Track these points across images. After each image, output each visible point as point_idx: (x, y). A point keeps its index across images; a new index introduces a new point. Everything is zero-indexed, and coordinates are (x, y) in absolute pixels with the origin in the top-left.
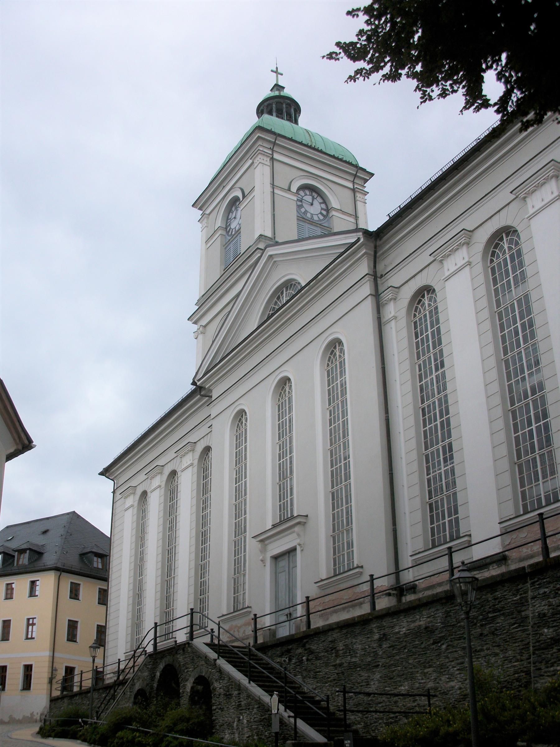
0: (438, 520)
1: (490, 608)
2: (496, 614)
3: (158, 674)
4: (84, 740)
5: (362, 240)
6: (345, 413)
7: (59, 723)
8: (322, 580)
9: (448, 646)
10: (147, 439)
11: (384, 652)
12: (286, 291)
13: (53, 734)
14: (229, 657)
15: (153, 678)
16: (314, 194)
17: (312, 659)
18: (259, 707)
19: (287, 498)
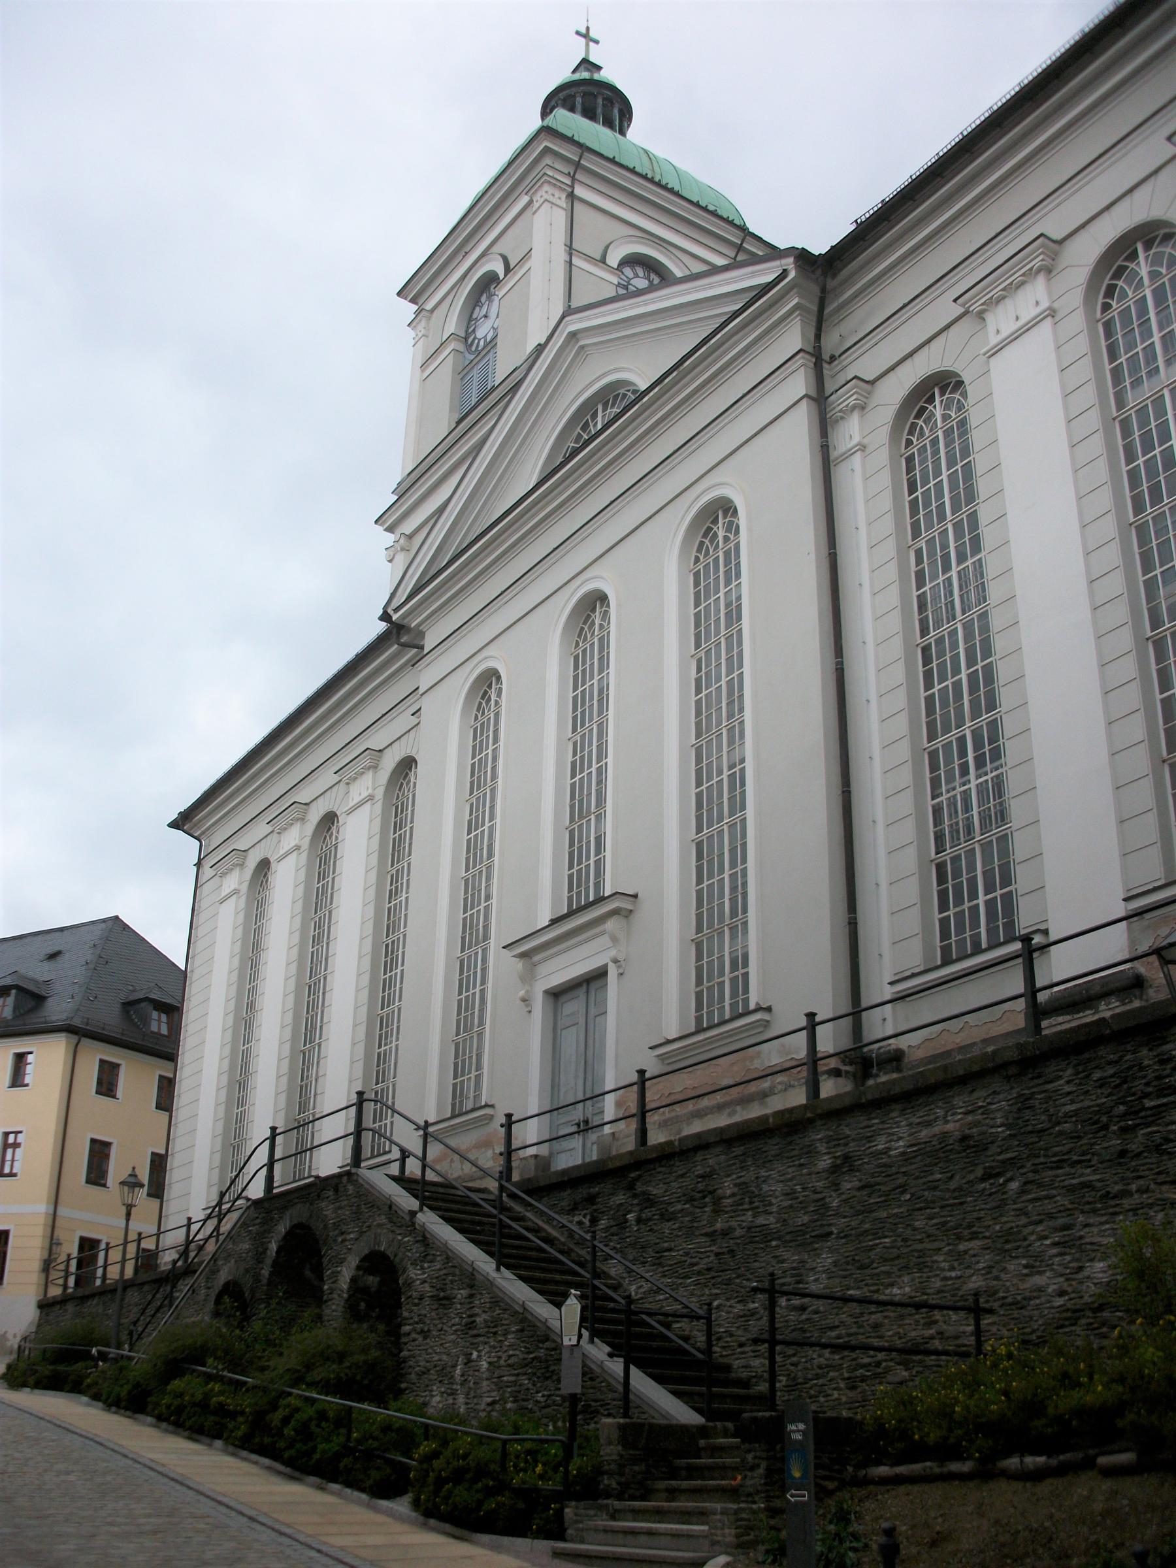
0: (959, 901)
1: (1147, 1084)
2: (1165, 1100)
3: (273, 1247)
4: (96, 1397)
5: (792, 274)
6: (735, 662)
7: (48, 1355)
8: (669, 1042)
9: (1025, 1183)
10: (273, 748)
11: (846, 1201)
12: (604, 410)
13: (31, 1380)
14: (446, 1210)
15: (260, 1256)
16: (652, 276)
17: (649, 1219)
18: (522, 1330)
19: (588, 858)
